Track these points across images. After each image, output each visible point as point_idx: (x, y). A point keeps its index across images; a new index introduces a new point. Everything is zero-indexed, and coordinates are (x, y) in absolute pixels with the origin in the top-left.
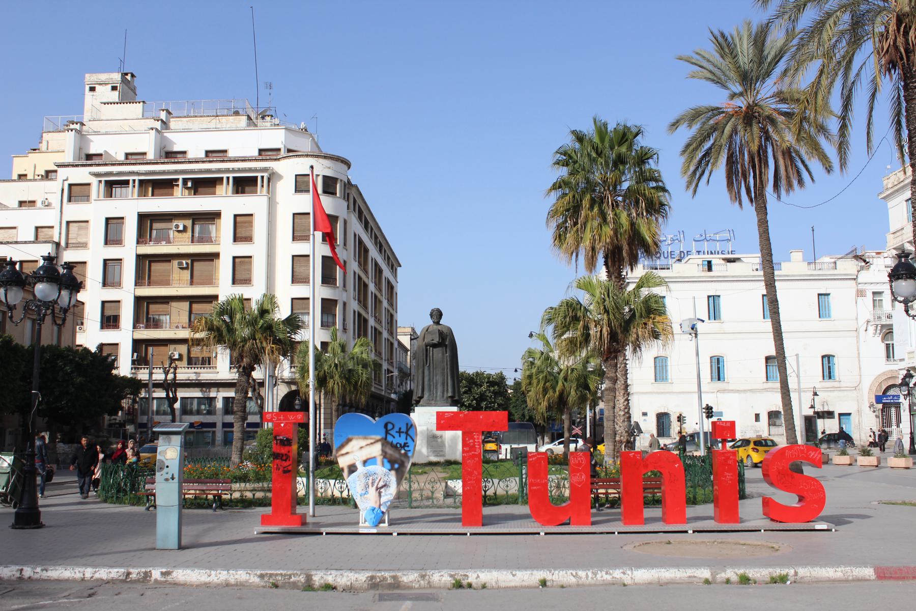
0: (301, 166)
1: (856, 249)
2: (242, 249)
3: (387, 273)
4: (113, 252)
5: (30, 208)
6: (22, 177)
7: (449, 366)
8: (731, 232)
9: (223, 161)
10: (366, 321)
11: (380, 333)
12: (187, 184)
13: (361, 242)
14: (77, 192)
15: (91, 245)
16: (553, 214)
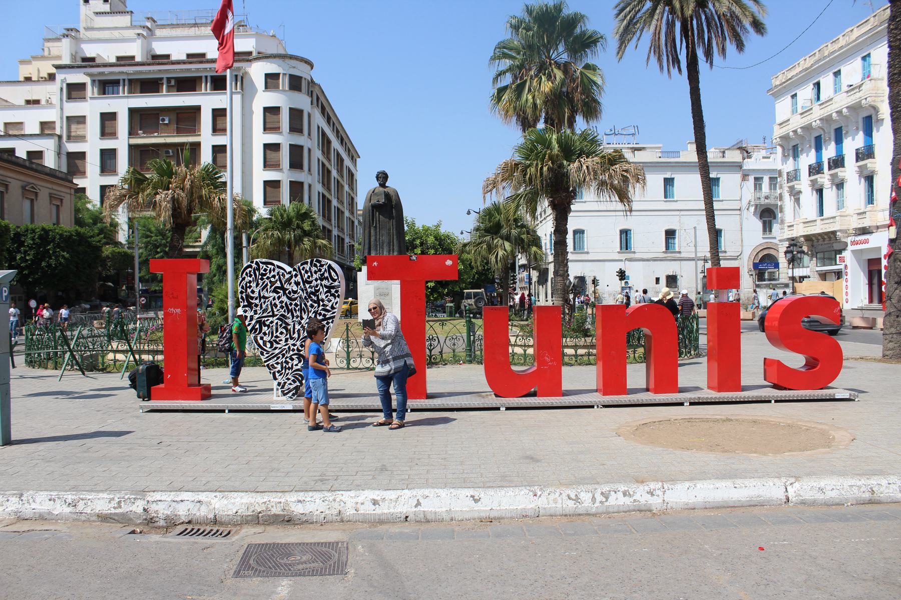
0: (271, 67)
1: (741, 141)
2: (220, 140)
3: (347, 162)
4: (108, 144)
5: (35, 106)
6: (28, 79)
7: (394, 226)
8: (636, 128)
9: (201, 62)
10: (329, 202)
11: (343, 213)
12: (170, 83)
13: (324, 134)
14: (75, 91)
15: (88, 137)
16: (503, 51)
